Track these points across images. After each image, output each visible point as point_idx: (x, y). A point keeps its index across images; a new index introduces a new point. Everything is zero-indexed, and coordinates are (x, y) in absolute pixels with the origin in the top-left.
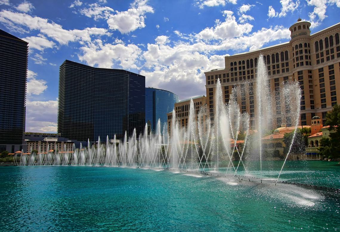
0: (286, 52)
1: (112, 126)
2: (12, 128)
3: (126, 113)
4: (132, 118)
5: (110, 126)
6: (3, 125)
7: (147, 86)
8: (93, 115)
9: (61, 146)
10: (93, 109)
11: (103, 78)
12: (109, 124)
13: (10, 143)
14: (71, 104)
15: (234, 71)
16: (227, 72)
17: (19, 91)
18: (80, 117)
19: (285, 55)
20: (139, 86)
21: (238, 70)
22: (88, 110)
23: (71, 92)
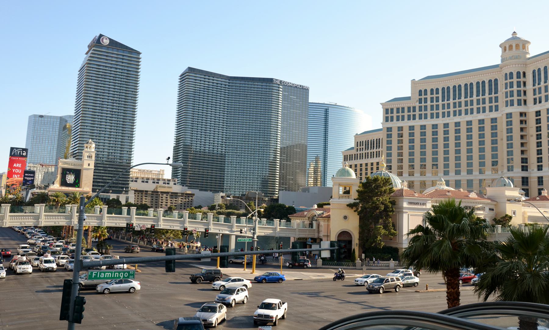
0: (496, 80)
6: (111, 132)
7: (310, 102)
15: (423, 104)
16: (414, 105)
17: (130, 84)
19: (494, 85)
21: (429, 103)
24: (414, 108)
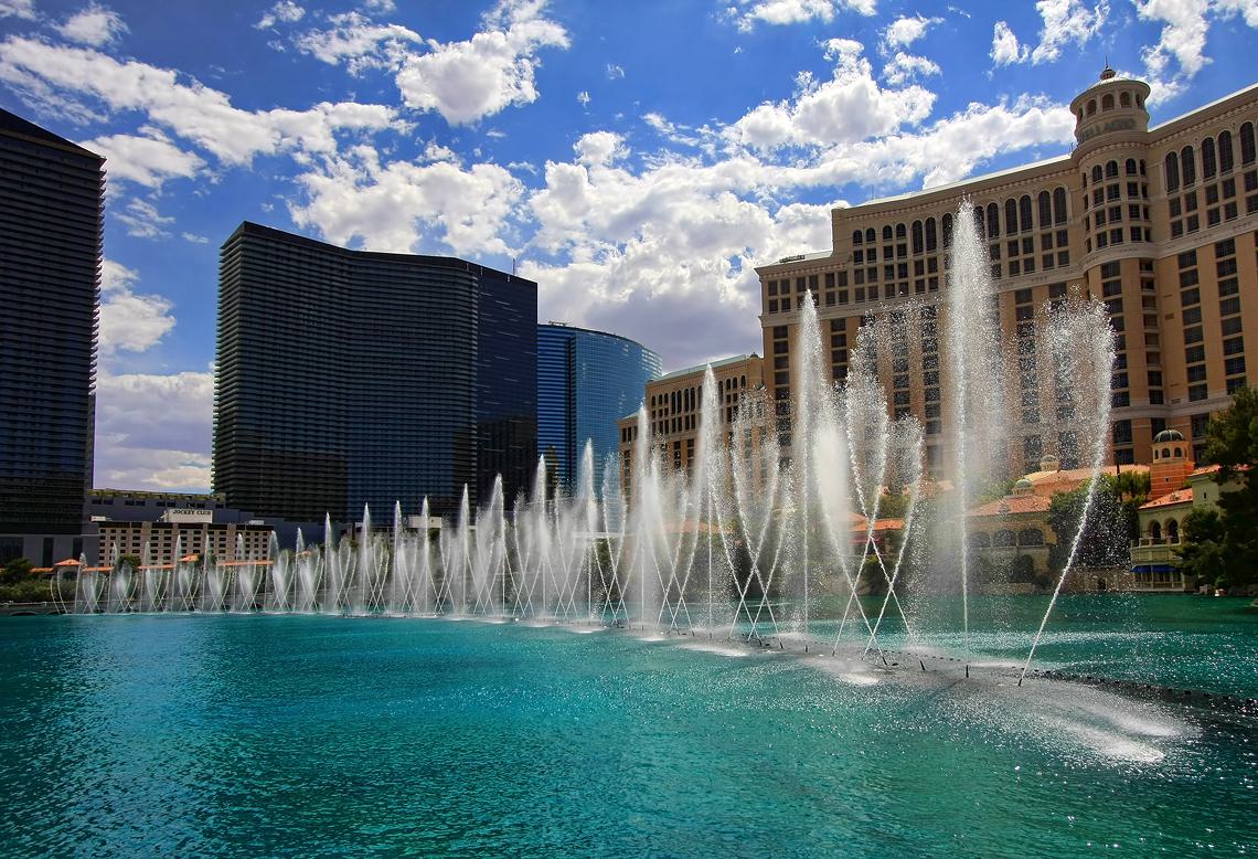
0: (1060, 193)
1: (414, 467)
2: (44, 474)
3: (466, 420)
4: (487, 436)
5: (405, 466)
6: (13, 462)
7: (543, 318)
8: (343, 425)
9: (224, 539)
10: (342, 402)
11: (381, 290)
12: (405, 461)
13: (36, 530)
14: (262, 383)
15: (865, 264)
16: (841, 268)
18: (295, 435)
19: (1053, 204)
20: (516, 317)
21: (880, 260)
22: (325, 405)
23: (263, 342)
24: (843, 275)
